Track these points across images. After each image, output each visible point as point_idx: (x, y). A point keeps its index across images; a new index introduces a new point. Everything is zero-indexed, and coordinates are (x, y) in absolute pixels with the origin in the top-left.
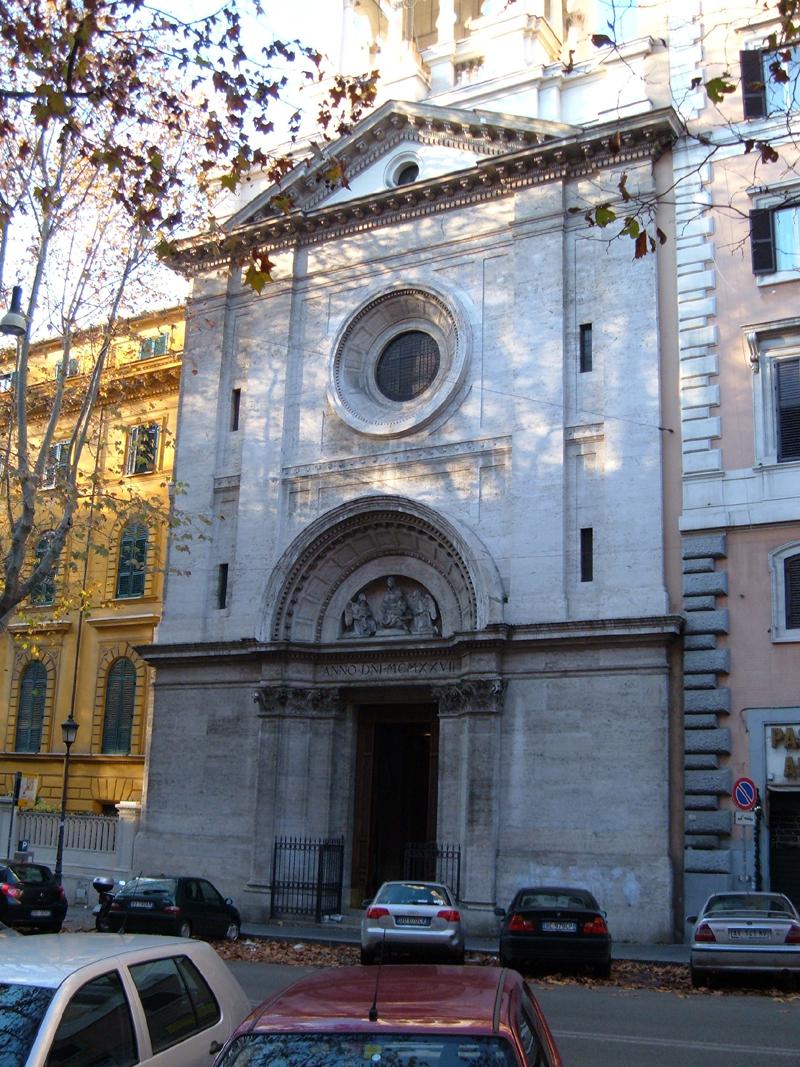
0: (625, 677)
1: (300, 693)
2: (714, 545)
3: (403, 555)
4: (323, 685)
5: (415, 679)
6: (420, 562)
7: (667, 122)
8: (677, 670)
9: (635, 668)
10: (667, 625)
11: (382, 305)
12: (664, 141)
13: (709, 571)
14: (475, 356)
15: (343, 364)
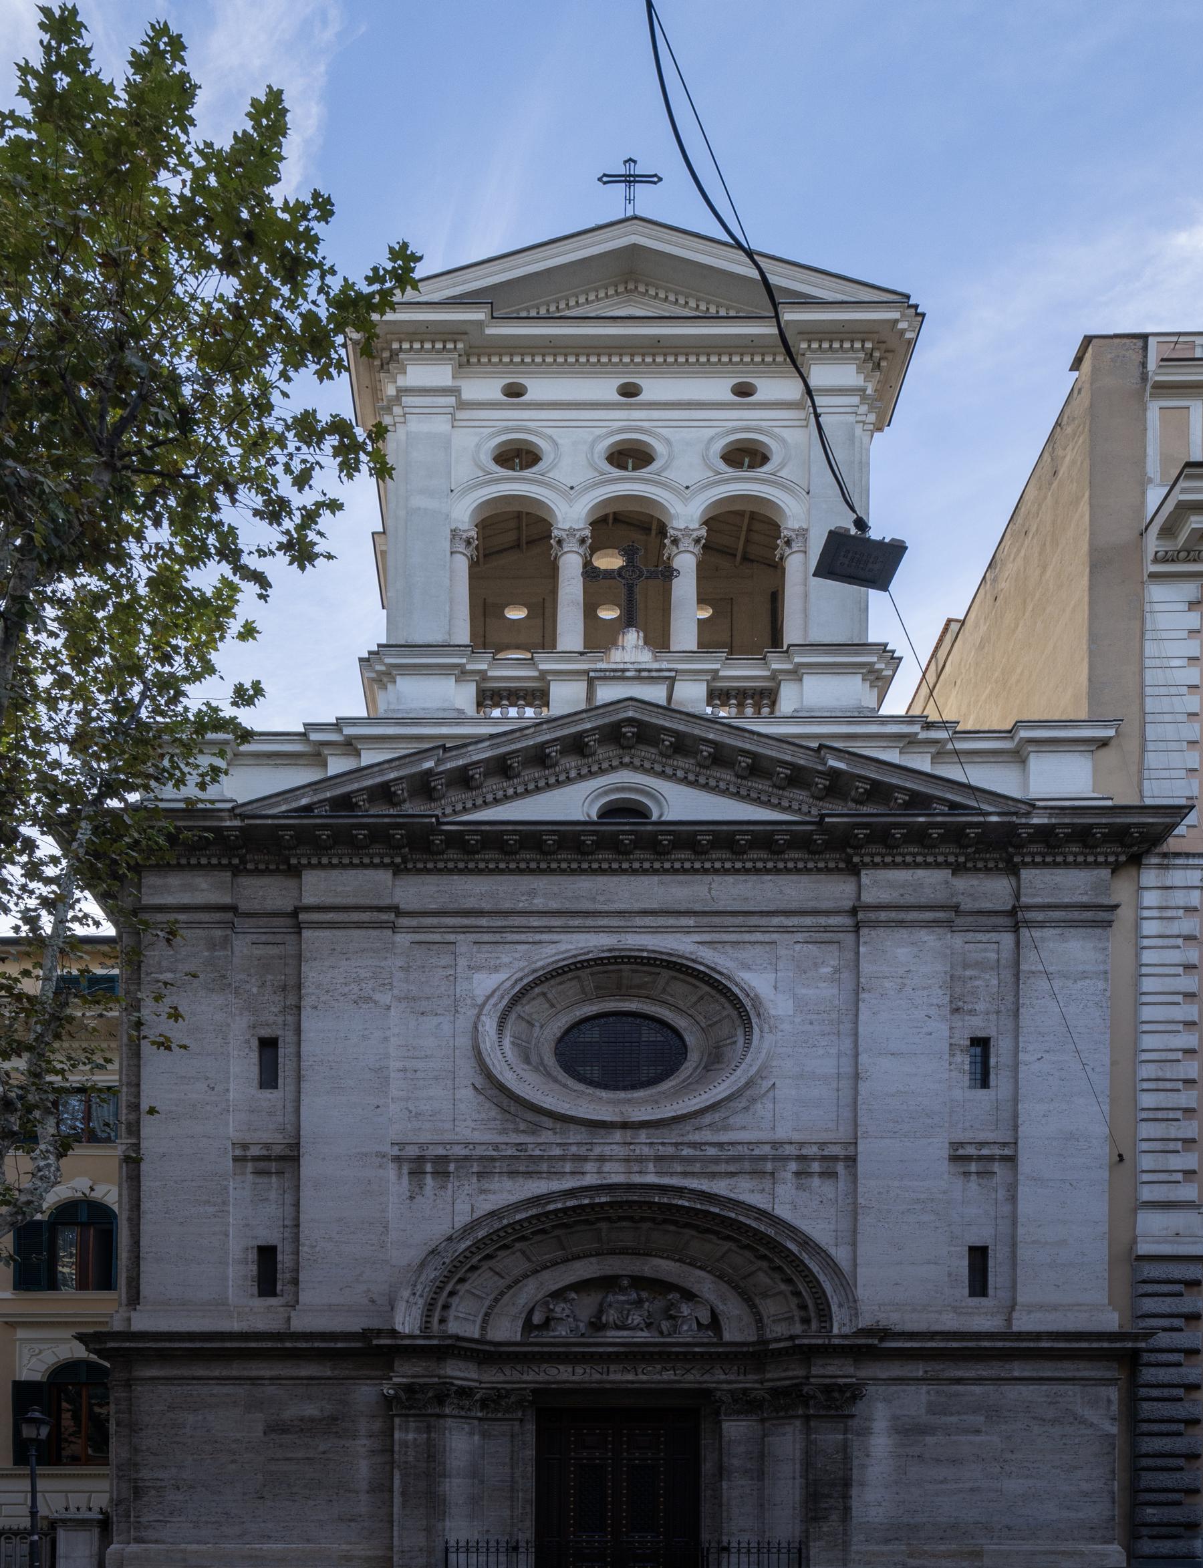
3: (647, 1255)
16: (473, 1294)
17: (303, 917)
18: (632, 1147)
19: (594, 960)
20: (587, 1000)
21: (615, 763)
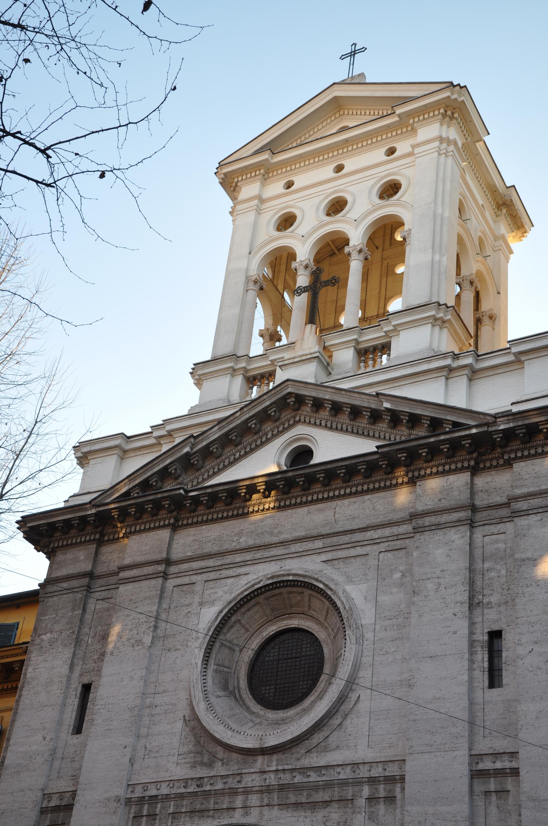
18: (265, 776)
19: (264, 587)
20: (269, 622)
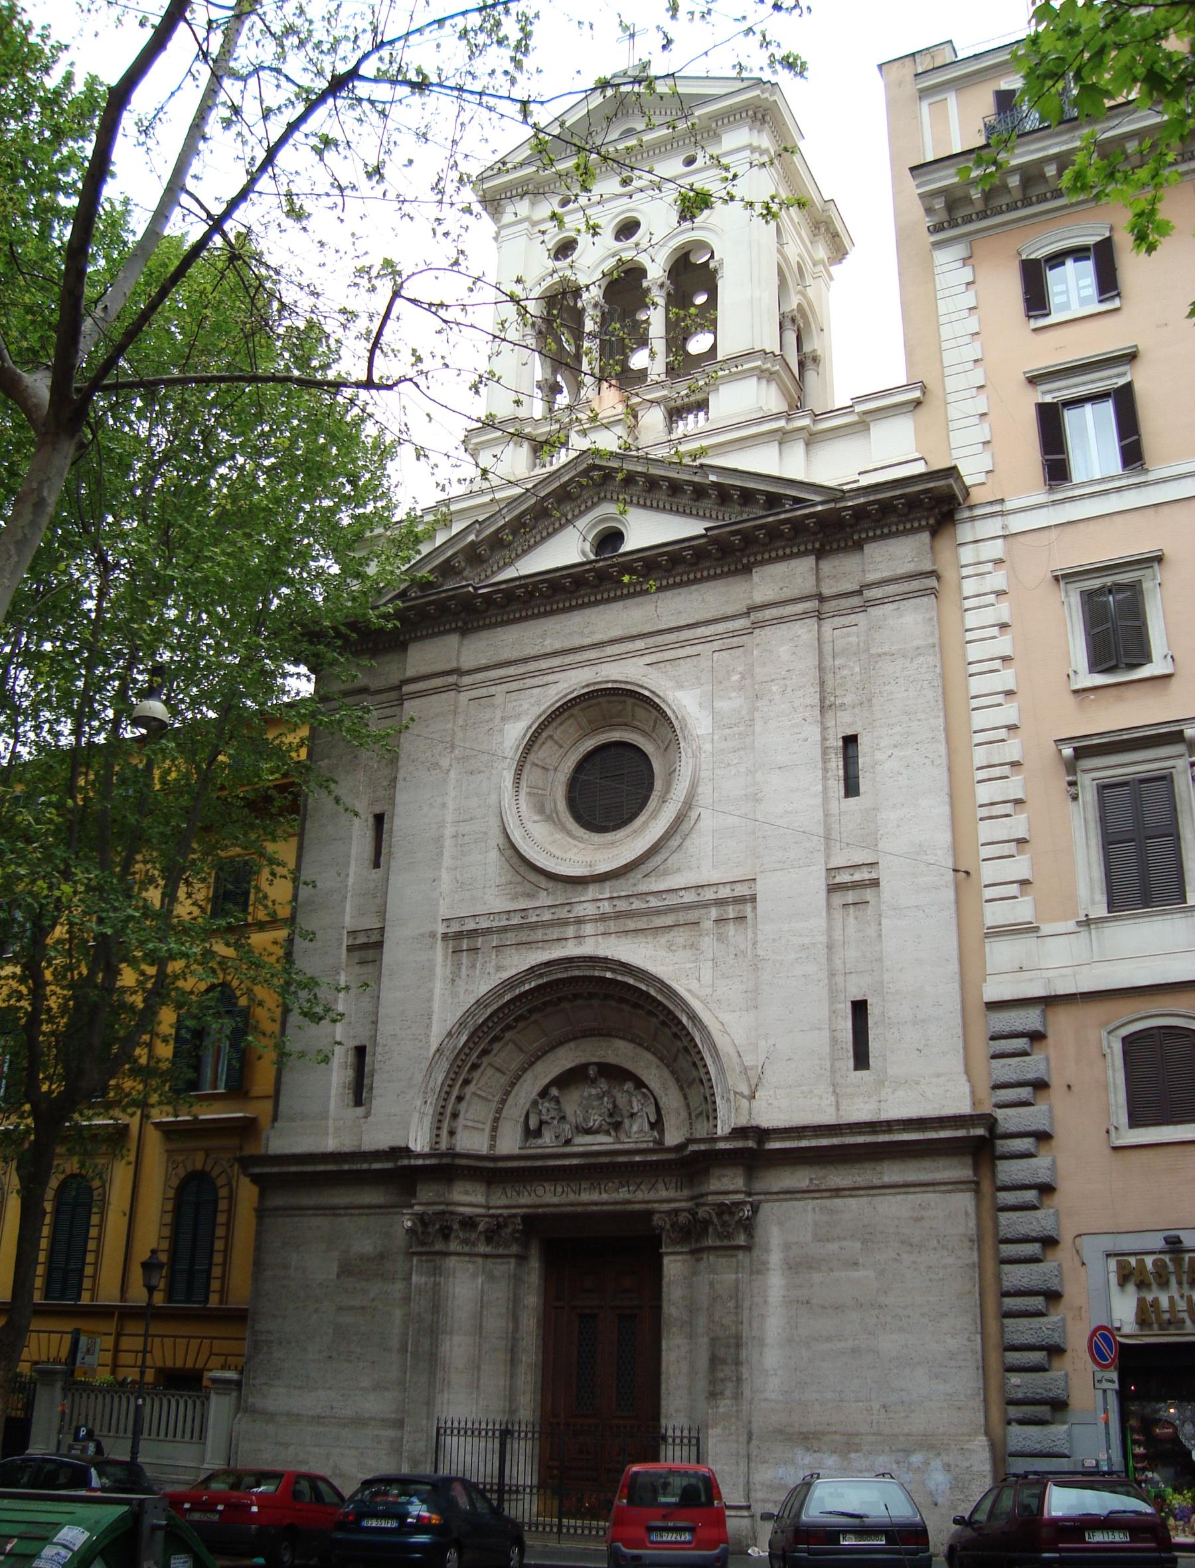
0: (919, 1195)
1: (469, 1223)
2: (1030, 1019)
4: (500, 1211)
5: (629, 1202)
6: (632, 1046)
7: (950, 486)
8: (986, 1187)
9: (933, 1184)
10: (974, 1126)
11: (577, 708)
12: (945, 509)
13: (1025, 1054)
14: (703, 774)
15: (523, 784)
16: (479, 1096)
17: (406, 689)
20: (594, 731)
21: (595, 500)
